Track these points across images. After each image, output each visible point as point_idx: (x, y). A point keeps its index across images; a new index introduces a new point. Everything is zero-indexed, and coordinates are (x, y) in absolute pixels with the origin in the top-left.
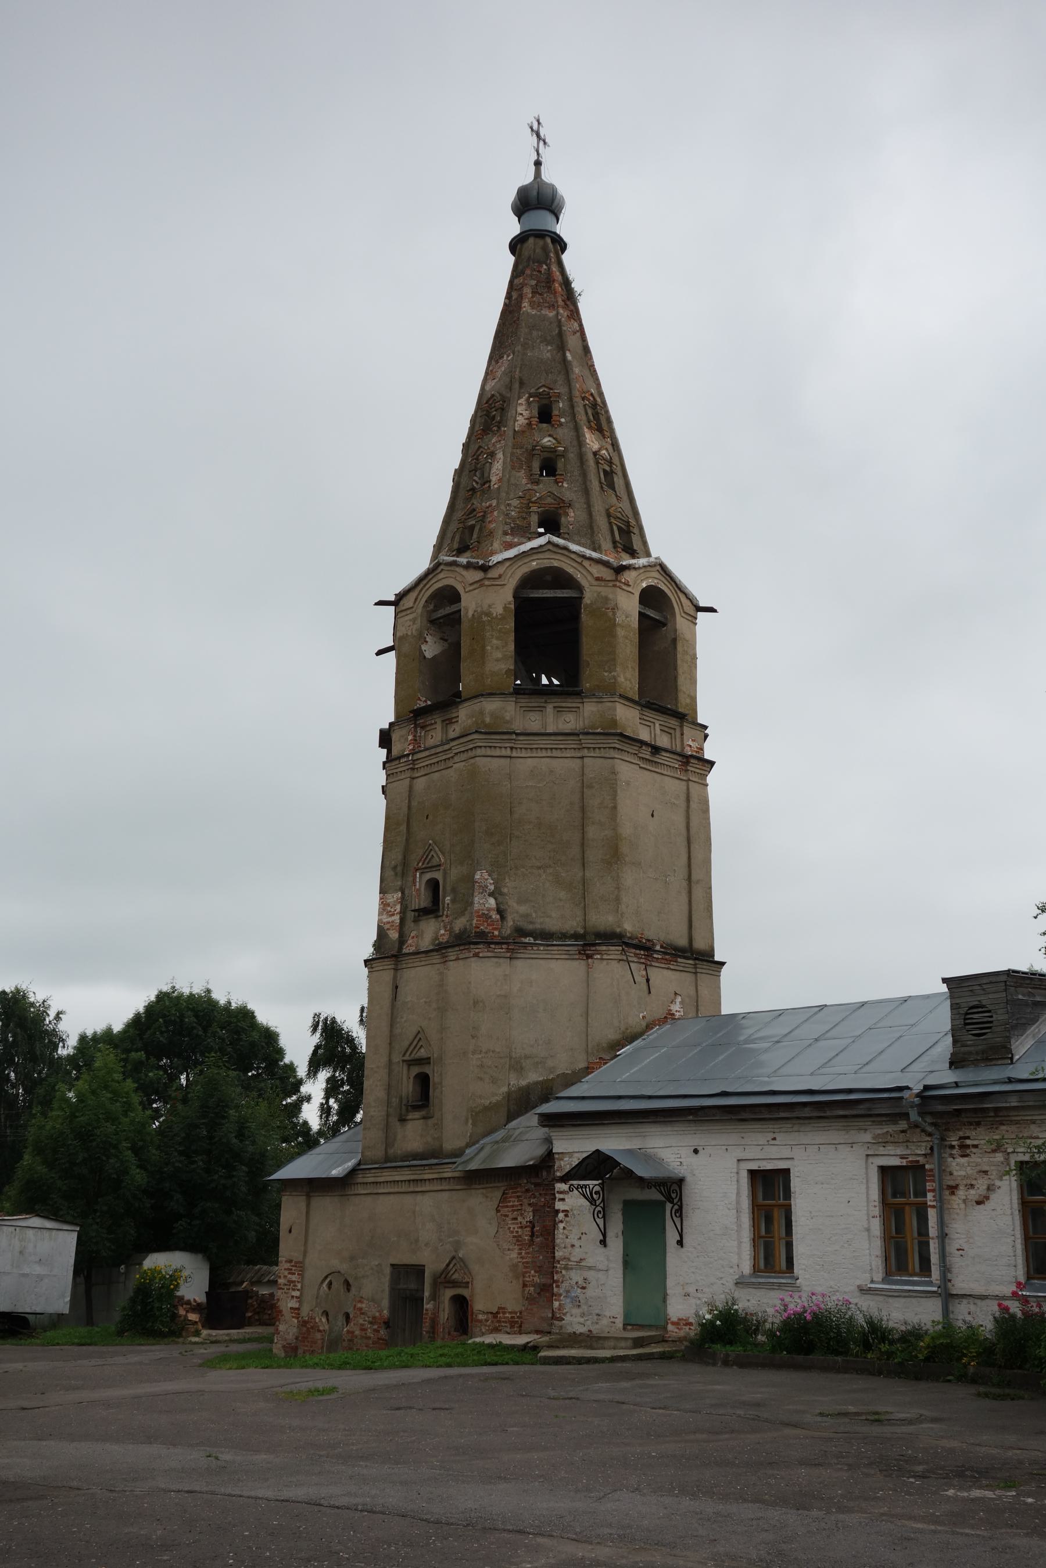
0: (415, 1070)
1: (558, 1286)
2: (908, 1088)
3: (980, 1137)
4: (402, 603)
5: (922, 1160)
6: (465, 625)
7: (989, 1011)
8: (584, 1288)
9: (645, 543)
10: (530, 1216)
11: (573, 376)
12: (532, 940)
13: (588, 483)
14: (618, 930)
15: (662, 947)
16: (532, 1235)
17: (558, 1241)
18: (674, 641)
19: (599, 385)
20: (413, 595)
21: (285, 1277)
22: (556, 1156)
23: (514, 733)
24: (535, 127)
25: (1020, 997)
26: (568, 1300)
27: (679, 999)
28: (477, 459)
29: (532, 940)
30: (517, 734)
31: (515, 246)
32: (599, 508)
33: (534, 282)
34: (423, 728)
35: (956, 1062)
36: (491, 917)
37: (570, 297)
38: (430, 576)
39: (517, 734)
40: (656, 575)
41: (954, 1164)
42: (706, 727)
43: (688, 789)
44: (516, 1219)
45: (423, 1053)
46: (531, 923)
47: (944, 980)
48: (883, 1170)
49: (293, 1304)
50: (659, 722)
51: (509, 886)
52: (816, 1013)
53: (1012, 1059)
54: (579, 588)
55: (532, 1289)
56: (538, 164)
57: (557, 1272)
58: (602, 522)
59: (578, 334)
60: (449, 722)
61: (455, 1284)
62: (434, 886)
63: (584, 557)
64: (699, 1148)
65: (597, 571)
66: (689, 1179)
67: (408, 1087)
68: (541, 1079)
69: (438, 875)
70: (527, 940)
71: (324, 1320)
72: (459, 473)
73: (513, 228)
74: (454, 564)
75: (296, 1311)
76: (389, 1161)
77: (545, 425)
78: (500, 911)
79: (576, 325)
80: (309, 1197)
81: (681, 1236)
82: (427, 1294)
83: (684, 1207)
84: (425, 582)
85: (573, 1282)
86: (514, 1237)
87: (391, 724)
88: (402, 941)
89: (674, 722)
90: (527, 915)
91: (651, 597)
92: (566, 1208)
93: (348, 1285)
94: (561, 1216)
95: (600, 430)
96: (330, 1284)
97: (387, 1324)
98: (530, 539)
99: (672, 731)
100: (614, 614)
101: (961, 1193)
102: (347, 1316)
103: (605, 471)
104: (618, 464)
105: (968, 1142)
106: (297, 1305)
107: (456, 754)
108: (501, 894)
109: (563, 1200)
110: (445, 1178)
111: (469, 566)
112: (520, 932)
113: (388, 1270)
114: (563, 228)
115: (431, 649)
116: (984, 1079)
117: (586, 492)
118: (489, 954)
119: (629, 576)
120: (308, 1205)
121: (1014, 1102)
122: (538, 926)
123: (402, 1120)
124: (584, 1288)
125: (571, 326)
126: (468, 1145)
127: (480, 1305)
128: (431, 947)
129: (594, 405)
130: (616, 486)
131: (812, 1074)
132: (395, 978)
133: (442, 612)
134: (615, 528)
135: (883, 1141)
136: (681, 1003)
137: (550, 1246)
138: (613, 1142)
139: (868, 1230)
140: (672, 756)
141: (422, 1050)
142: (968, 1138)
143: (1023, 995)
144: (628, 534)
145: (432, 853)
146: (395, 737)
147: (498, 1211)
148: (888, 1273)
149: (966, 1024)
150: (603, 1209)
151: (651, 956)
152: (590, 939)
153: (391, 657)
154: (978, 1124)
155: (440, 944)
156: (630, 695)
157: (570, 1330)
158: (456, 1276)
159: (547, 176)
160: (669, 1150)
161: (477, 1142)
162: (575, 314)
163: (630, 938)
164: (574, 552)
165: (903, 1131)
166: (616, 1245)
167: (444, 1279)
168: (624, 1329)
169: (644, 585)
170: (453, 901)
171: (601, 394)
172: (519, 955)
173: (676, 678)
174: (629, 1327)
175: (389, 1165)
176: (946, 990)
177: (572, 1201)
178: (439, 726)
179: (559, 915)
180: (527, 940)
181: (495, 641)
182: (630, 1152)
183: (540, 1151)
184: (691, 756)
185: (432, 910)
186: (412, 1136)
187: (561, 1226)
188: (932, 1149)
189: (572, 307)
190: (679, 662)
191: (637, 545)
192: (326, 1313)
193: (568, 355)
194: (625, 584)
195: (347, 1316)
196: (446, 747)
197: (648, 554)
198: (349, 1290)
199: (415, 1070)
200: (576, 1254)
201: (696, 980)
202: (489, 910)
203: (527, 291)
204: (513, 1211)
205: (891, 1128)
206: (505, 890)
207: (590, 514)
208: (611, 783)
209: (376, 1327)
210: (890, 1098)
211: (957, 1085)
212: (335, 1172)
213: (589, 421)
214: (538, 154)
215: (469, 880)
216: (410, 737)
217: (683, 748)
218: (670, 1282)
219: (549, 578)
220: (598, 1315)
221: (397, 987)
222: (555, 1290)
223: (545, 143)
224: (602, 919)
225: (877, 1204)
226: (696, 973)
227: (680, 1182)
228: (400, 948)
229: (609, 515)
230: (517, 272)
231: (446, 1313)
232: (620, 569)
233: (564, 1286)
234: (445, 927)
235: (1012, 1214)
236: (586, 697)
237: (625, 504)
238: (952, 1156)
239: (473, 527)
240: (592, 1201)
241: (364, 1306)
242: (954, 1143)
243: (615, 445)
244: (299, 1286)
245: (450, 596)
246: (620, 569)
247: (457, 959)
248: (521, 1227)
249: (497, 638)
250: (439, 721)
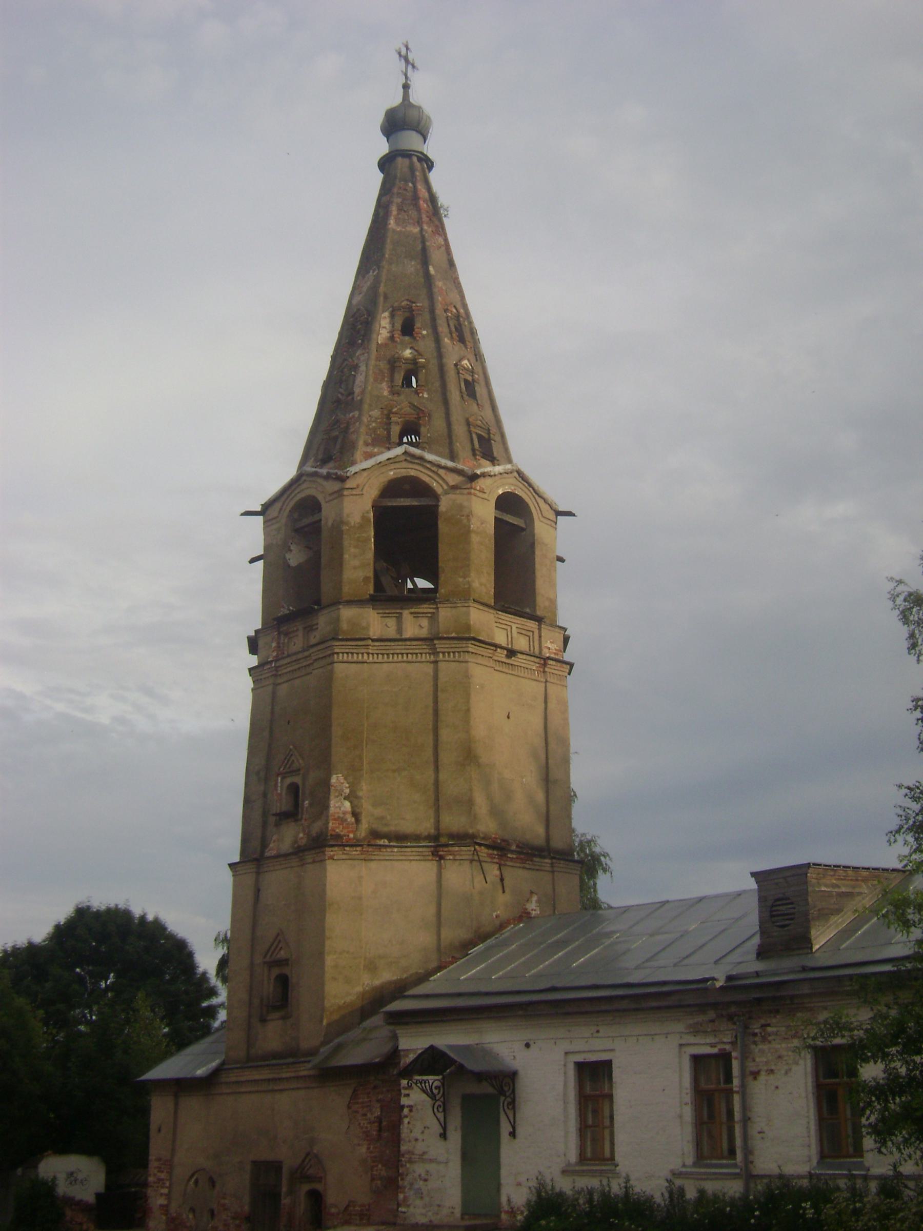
0: (276, 971)
1: (402, 1179)
2: (714, 979)
3: (777, 1025)
4: (268, 512)
5: (728, 1047)
6: (325, 534)
7: (792, 903)
8: (426, 1180)
9: (506, 450)
10: (377, 1112)
11: (436, 290)
12: (386, 842)
13: (448, 394)
14: (471, 831)
15: (518, 846)
16: (380, 1130)
17: (403, 1136)
18: (532, 545)
19: (463, 297)
20: (278, 506)
21: (155, 1175)
22: (402, 1053)
23: (369, 638)
24: (404, 52)
25: (823, 889)
26: (412, 1192)
27: (535, 898)
28: (342, 372)
29: (386, 842)
30: (373, 640)
31: (385, 164)
32: (457, 417)
33: (399, 200)
34: (287, 634)
35: (762, 954)
36: (346, 820)
37: (435, 212)
38: (294, 487)
39: (373, 640)
40: (513, 481)
41: (757, 1050)
42: (565, 629)
43: (546, 690)
44: (365, 1115)
45: (283, 954)
46: (386, 825)
47: (753, 874)
48: (697, 1059)
49: (162, 1201)
50: (516, 623)
51: (364, 789)
52: (656, 910)
53: (811, 948)
54: (436, 497)
55: (379, 1182)
56: (406, 87)
57: (402, 1166)
58: (460, 430)
59: (443, 249)
60: (310, 629)
61: (309, 1179)
62: (294, 790)
63: (439, 466)
64: (531, 1043)
65: (453, 479)
66: (521, 1073)
67: (269, 988)
68: (395, 978)
69: (297, 779)
70: (381, 842)
71: (191, 1216)
72: (327, 386)
73: (383, 147)
74: (315, 474)
75: (165, 1208)
76: (253, 1059)
77: (407, 338)
78: (356, 815)
79: (441, 240)
80: (176, 1096)
81: (514, 1128)
82: (284, 1189)
83: (517, 1099)
84: (288, 493)
85: (416, 1175)
86: (364, 1132)
87: (257, 632)
88: (264, 845)
89: (532, 625)
90: (382, 818)
91: (509, 503)
92: (411, 1103)
93: (212, 1182)
94: (406, 1111)
95: (462, 340)
96: (196, 1182)
97: (248, 1219)
98: (389, 449)
99: (530, 634)
100: (469, 520)
101: (763, 1077)
102: (212, 1214)
103: (466, 381)
104: (481, 372)
105: (769, 1029)
106: (165, 1202)
107: (316, 660)
108: (357, 797)
109: (408, 1095)
110: (301, 1077)
111: (328, 477)
112: (376, 834)
113: (248, 1167)
114: (431, 149)
115: (296, 557)
116: (783, 968)
117: (446, 402)
118: (344, 857)
119: (481, 483)
120: (176, 1105)
121: (806, 990)
122: (392, 828)
123: (263, 1020)
124: (426, 1180)
125: (434, 242)
126: (324, 1043)
127: (334, 1198)
128: (291, 851)
129: (458, 316)
130: (478, 395)
131: (675, 965)
132: (257, 881)
133: (306, 521)
134: (474, 436)
135: (696, 1030)
136: (538, 901)
137: (396, 1140)
138: (447, 1038)
139: (681, 1116)
140: (528, 658)
141: (282, 952)
142: (769, 1025)
143: (826, 886)
144: (488, 443)
145: (293, 758)
146: (261, 643)
147: (349, 1107)
148: (700, 1157)
149: (772, 916)
150: (444, 1103)
151: (505, 855)
152: (443, 840)
153: (260, 564)
154: (777, 1011)
155: (299, 847)
156: (485, 600)
157: (413, 1221)
158: (311, 1171)
159: (414, 99)
160: (503, 1044)
161: (331, 1041)
162: (440, 229)
163: (483, 838)
164: (430, 462)
165: (712, 1021)
166: (455, 1137)
167: (300, 1175)
168: (462, 1218)
169: (500, 492)
170: (311, 805)
171: (465, 306)
172: (373, 857)
173: (534, 581)
174: (466, 1217)
175: (250, 1064)
176: (755, 886)
177: (414, 1097)
178: (300, 633)
179: (414, 817)
180: (381, 842)
181: (353, 550)
182: (467, 1048)
183: (387, 1048)
184: (549, 658)
185: (291, 815)
186: (272, 1036)
187: (406, 1121)
188: (736, 1037)
189: (437, 223)
190: (537, 566)
191: (497, 451)
192: (192, 1210)
193: (431, 269)
194: (480, 491)
195: (212, 1214)
196: (306, 654)
197: (510, 461)
198: (214, 1186)
199: (276, 971)
200: (420, 1148)
201: (553, 879)
202: (344, 813)
203: (394, 210)
204: (363, 1107)
205: (700, 1018)
206: (360, 794)
207: (449, 424)
208: (464, 686)
209: (237, 1222)
210: (698, 989)
211: (757, 974)
212: (200, 1072)
213: (451, 333)
214: (406, 78)
215: (326, 784)
216: (274, 645)
217: (540, 652)
218: (504, 1172)
219: (407, 487)
220: (439, 1206)
221: (259, 890)
222: (401, 1183)
223: (413, 66)
224: (453, 821)
225: (688, 1091)
226: (553, 872)
227: (513, 1075)
228: (262, 852)
229: (468, 424)
230: (386, 189)
231: (302, 1207)
232: (474, 478)
233: (409, 1178)
234: (304, 831)
235: (807, 1097)
236: (440, 603)
237: (488, 413)
238: (755, 1043)
239: (336, 438)
240: (433, 1097)
241: (226, 1201)
242: (756, 1031)
243: (478, 356)
244: (167, 1184)
245: (311, 506)
246: (474, 478)
247: (314, 862)
248: (370, 1123)
249: (356, 547)
250: (300, 628)
